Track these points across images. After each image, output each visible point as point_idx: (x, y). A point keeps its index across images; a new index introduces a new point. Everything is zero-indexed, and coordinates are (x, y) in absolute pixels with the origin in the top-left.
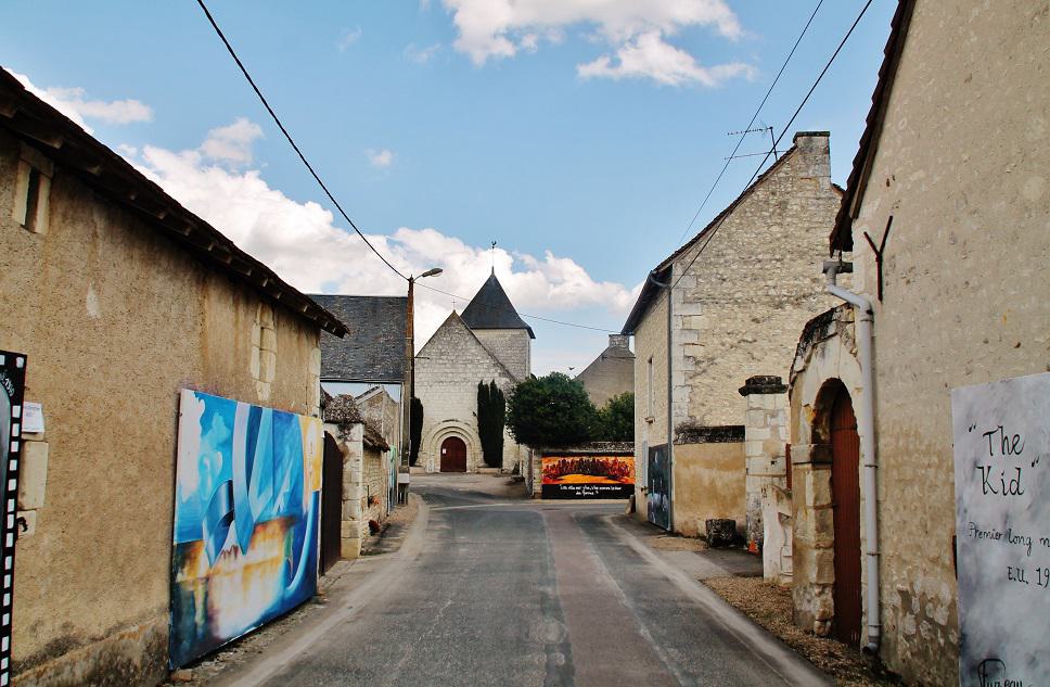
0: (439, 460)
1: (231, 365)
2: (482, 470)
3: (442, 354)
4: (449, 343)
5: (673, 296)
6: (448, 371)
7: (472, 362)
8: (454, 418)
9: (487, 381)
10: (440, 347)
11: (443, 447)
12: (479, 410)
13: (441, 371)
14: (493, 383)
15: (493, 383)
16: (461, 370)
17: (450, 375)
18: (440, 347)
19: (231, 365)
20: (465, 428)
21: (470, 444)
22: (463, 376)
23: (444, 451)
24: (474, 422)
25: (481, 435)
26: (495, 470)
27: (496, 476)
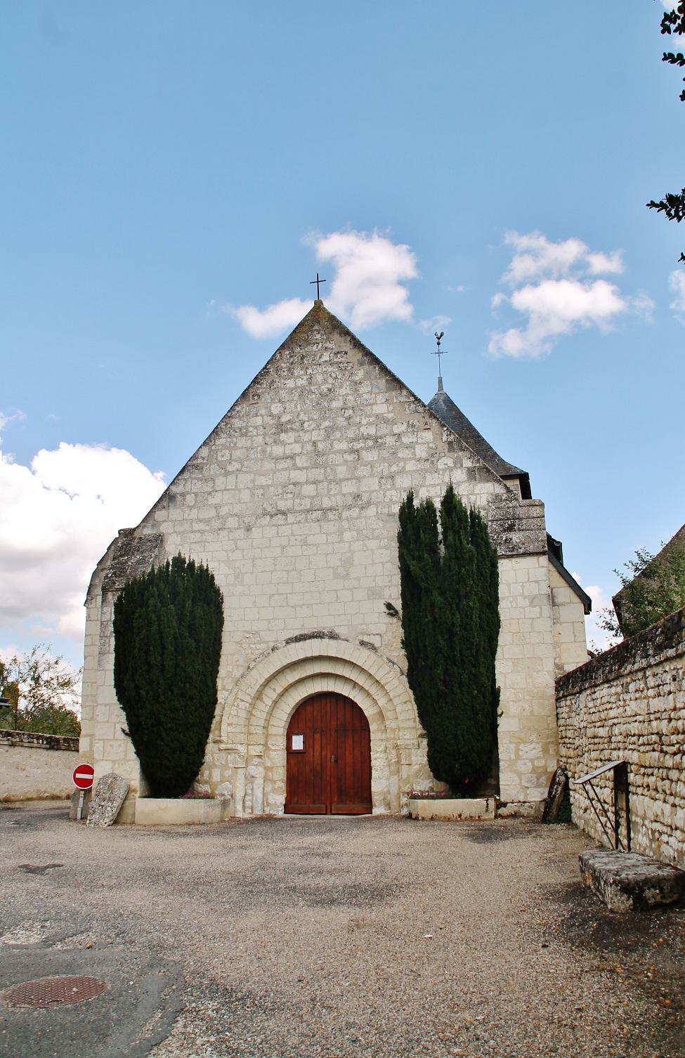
0: (280, 774)
1: (205, 568)
2: (426, 807)
3: (281, 428)
4: (303, 393)
5: (275, 724)
6: (300, 476)
7: (377, 441)
8: (324, 624)
9: (431, 492)
10: (276, 408)
11: (293, 727)
12: (130, 723)
13: (282, 477)
14: (450, 500)
15: (450, 500)
16: (342, 471)
17: (309, 490)
18: (276, 408)
19: (205, 568)
20: (362, 657)
21: (381, 715)
22: (349, 488)
23: (298, 743)
24: (391, 633)
25: (417, 678)
26: (471, 806)
27: (484, 834)
